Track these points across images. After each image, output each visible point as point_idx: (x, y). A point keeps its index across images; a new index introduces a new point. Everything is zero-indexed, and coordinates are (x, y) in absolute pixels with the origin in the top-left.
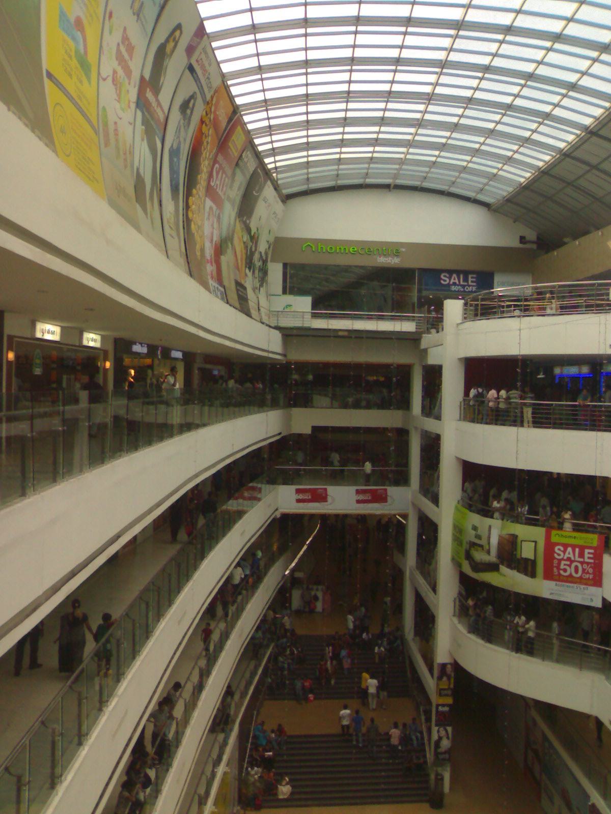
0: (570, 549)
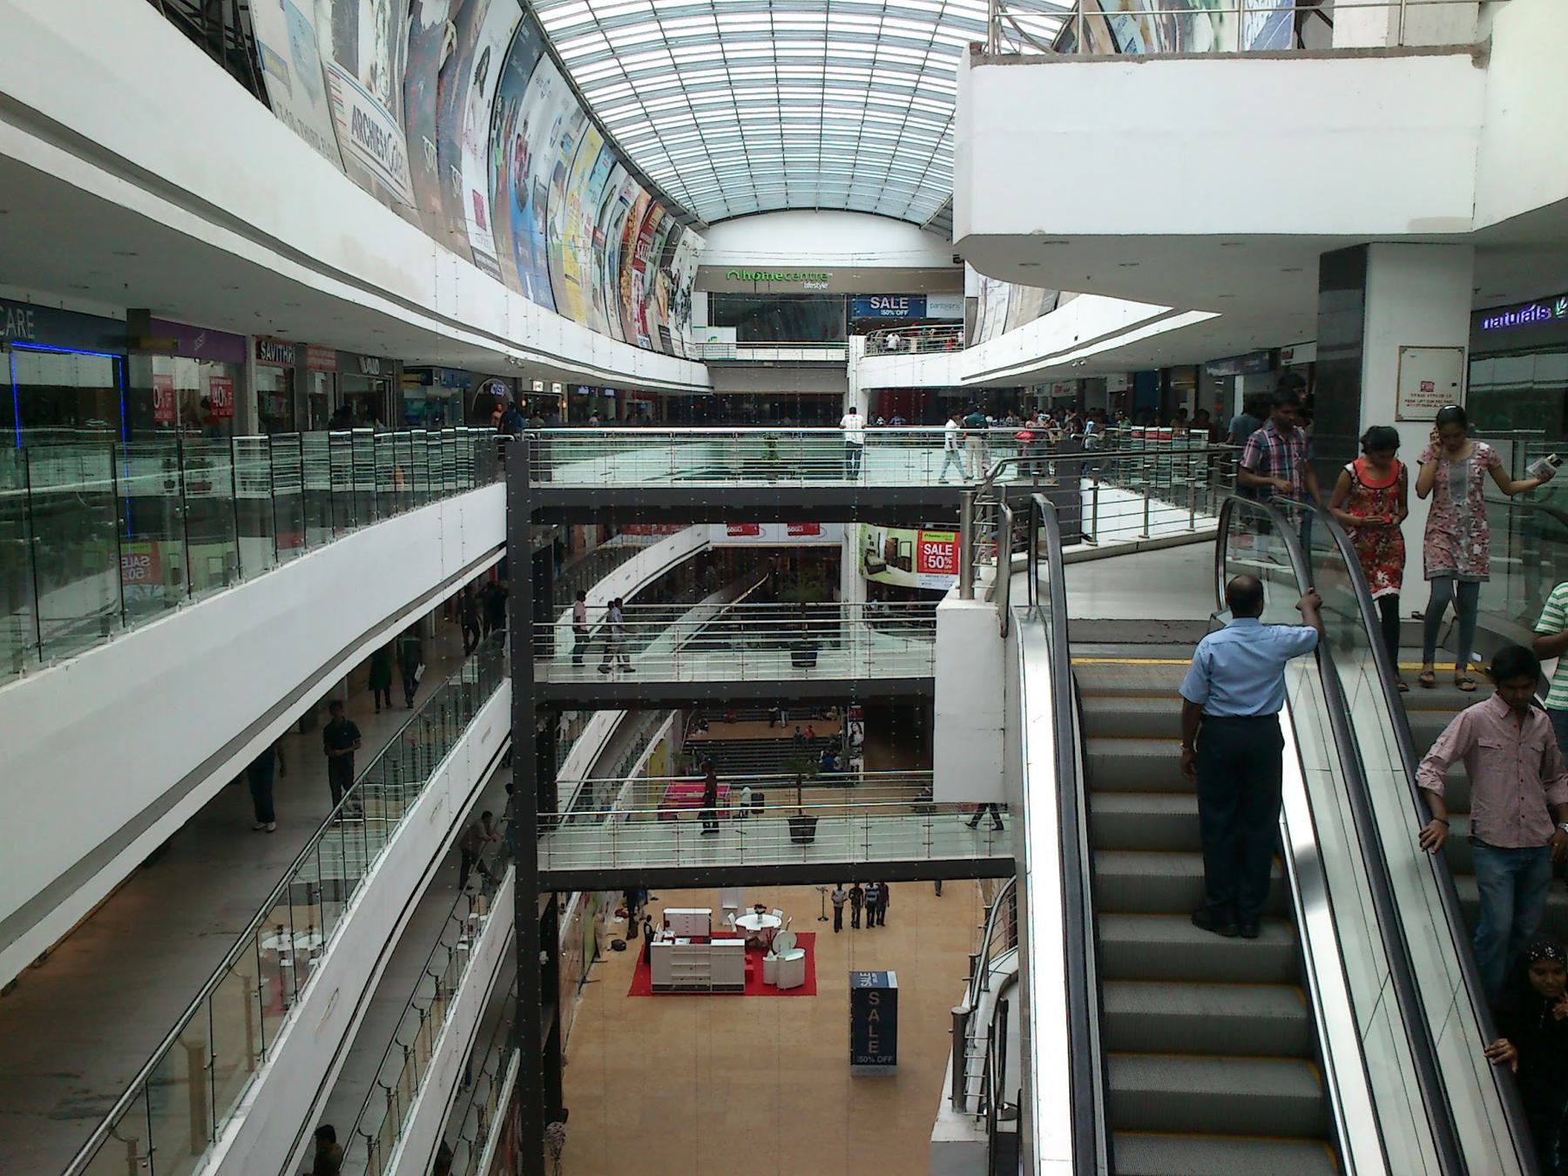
0: (935, 546)
